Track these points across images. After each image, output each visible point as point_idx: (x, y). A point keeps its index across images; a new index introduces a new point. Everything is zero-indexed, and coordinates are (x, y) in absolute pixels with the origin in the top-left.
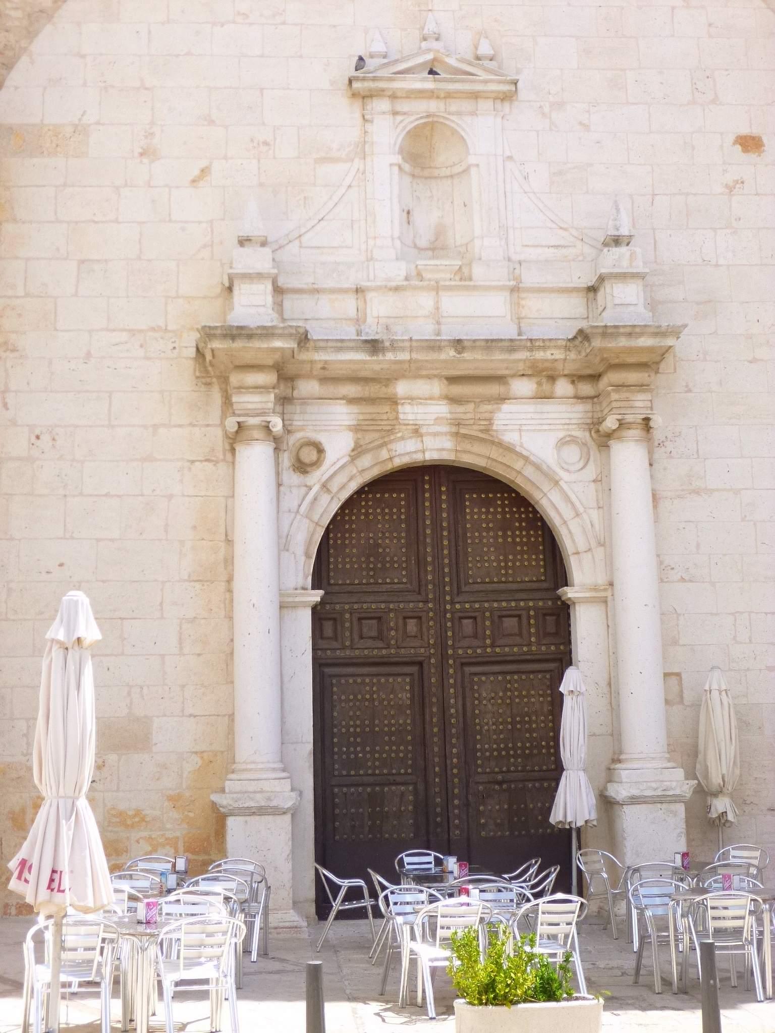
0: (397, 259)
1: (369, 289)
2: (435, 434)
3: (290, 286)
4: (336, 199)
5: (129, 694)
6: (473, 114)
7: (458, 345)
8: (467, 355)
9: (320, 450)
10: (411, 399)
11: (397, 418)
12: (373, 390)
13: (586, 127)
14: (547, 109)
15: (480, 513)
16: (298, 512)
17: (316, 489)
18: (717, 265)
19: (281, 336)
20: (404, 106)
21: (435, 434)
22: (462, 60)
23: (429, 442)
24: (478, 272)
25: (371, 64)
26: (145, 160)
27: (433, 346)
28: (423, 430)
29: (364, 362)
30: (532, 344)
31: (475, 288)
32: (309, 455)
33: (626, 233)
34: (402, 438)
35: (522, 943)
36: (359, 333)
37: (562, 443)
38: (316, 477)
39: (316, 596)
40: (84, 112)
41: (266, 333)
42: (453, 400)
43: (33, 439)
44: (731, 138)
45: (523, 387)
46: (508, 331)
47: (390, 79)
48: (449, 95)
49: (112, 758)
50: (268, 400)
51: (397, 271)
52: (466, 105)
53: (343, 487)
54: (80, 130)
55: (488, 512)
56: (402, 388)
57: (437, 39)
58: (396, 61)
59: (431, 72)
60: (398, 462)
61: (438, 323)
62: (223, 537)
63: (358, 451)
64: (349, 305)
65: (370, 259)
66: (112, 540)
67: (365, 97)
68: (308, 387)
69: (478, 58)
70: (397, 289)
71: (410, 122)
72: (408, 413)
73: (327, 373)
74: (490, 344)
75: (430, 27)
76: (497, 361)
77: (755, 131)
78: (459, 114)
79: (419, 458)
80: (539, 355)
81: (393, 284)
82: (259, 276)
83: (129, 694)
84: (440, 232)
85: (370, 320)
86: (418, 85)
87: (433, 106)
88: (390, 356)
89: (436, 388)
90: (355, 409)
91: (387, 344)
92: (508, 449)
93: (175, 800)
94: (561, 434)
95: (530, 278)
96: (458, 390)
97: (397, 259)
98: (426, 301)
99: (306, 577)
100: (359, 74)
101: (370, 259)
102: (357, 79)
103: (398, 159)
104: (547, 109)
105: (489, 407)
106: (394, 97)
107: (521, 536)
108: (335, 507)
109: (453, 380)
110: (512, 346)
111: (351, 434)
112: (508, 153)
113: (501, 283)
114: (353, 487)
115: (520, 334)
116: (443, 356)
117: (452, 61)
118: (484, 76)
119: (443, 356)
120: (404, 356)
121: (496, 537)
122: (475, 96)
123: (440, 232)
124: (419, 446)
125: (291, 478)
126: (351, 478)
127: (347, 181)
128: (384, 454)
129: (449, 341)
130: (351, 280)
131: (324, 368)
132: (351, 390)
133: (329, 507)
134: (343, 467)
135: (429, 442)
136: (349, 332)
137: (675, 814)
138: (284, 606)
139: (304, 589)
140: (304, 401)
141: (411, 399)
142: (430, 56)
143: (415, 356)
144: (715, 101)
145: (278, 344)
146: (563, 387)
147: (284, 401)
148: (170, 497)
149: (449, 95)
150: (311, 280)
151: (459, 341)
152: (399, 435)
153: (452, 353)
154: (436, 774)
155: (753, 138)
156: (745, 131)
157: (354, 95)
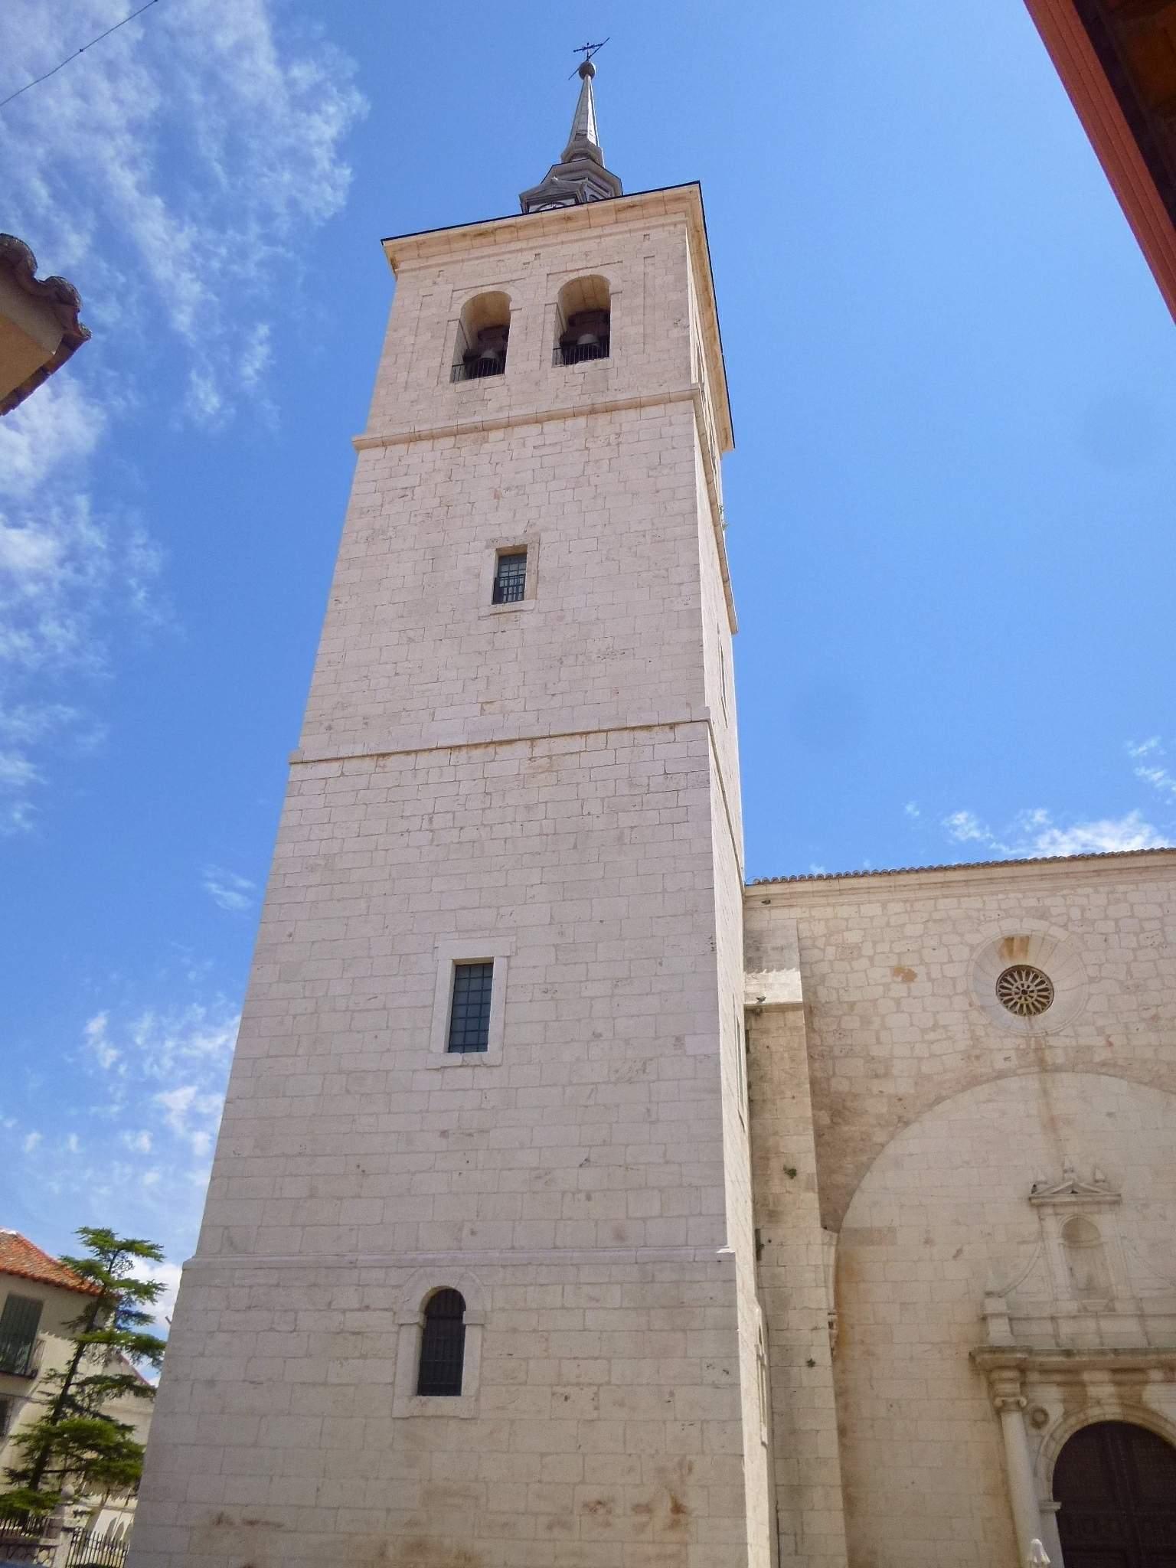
1: (1058, 1318)
2: (1110, 1404)
3: (1016, 1316)
6: (1099, 1212)
7: (1116, 1351)
8: (1122, 1358)
9: (1046, 1414)
10: (1093, 1383)
11: (1086, 1395)
13: (1164, 1218)
16: (1039, 1452)
17: (1047, 1439)
19: (1019, 1351)
20: (1060, 1210)
21: (1110, 1404)
22: (1088, 1184)
23: (1107, 1409)
24: (1118, 1306)
25: (1041, 1188)
26: (928, 1246)
27: (1102, 1353)
28: (1103, 1401)
29: (1062, 1362)
30: (1158, 1351)
31: (1119, 1316)
32: (1040, 1417)
34: (1091, 1407)
35: (1073, 933)
36: (1058, 1344)
38: (1046, 1431)
39: (1057, 1506)
40: (892, 1220)
41: (1013, 1349)
42: (1118, 1384)
46: (1141, 1343)
47: (1051, 1197)
48: (1083, 1204)
50: (1015, 1387)
51: (1072, 1307)
52: (1095, 1208)
53: (1062, 1437)
54: (892, 1230)
56: (1086, 1376)
57: (1072, 1171)
58: (1053, 1187)
59: (1073, 1192)
60: (1091, 1421)
61: (1101, 1337)
63: (1067, 1415)
64: (1049, 1327)
65: (1057, 1300)
67: (1040, 1206)
68: (1034, 1377)
69: (1097, 1181)
70: (1074, 1317)
71: (1066, 1219)
72: (1092, 1391)
74: (1134, 1351)
75: (1067, 1165)
76: (1139, 1361)
78: (1090, 1213)
79: (1102, 1418)
80: (1163, 1357)
82: (1000, 1315)
84: (1090, 1279)
86: (1068, 1199)
87: (1076, 1209)
88: (1077, 1358)
89: (1104, 1376)
90: (1061, 1389)
91: (1075, 1352)
92: (1154, 1413)
95: (1149, 1308)
96: (1119, 1377)
98: (1090, 1325)
99: (1049, 1493)
100: (1033, 1195)
101: (1057, 1300)
102: (1034, 1198)
103: (1061, 1241)
105: (1138, 1387)
106: (1054, 1205)
108: (1059, 1448)
109: (1115, 1371)
110: (1145, 1352)
111: (1061, 1405)
113: (1132, 1313)
114: (1067, 1436)
115: (1149, 1344)
116: (1108, 1358)
117: (1082, 1185)
118: (1103, 1193)
119: (1108, 1358)
120: (1085, 1358)
122: (1099, 1203)
123: (1090, 1279)
124: (1101, 1411)
125: (1033, 1431)
126: (1066, 1431)
127: (1036, 1254)
128: (1082, 1416)
129: (1111, 1349)
130: (1047, 1311)
131: (1040, 1365)
132: (1058, 1378)
133: (1056, 1449)
134: (1060, 1425)
135: (1107, 1409)
136: (1050, 1344)
138: (1042, 1512)
139: (1050, 1501)
140: (1033, 1384)
141: (1093, 1383)
142: (1071, 1183)
143: (1093, 1358)
145: (1019, 1355)
147: (1023, 1384)
149: (1083, 1204)
150: (1025, 1312)
151: (1116, 1350)
152: (1090, 1405)
153: (1113, 1356)
157: (1032, 1205)
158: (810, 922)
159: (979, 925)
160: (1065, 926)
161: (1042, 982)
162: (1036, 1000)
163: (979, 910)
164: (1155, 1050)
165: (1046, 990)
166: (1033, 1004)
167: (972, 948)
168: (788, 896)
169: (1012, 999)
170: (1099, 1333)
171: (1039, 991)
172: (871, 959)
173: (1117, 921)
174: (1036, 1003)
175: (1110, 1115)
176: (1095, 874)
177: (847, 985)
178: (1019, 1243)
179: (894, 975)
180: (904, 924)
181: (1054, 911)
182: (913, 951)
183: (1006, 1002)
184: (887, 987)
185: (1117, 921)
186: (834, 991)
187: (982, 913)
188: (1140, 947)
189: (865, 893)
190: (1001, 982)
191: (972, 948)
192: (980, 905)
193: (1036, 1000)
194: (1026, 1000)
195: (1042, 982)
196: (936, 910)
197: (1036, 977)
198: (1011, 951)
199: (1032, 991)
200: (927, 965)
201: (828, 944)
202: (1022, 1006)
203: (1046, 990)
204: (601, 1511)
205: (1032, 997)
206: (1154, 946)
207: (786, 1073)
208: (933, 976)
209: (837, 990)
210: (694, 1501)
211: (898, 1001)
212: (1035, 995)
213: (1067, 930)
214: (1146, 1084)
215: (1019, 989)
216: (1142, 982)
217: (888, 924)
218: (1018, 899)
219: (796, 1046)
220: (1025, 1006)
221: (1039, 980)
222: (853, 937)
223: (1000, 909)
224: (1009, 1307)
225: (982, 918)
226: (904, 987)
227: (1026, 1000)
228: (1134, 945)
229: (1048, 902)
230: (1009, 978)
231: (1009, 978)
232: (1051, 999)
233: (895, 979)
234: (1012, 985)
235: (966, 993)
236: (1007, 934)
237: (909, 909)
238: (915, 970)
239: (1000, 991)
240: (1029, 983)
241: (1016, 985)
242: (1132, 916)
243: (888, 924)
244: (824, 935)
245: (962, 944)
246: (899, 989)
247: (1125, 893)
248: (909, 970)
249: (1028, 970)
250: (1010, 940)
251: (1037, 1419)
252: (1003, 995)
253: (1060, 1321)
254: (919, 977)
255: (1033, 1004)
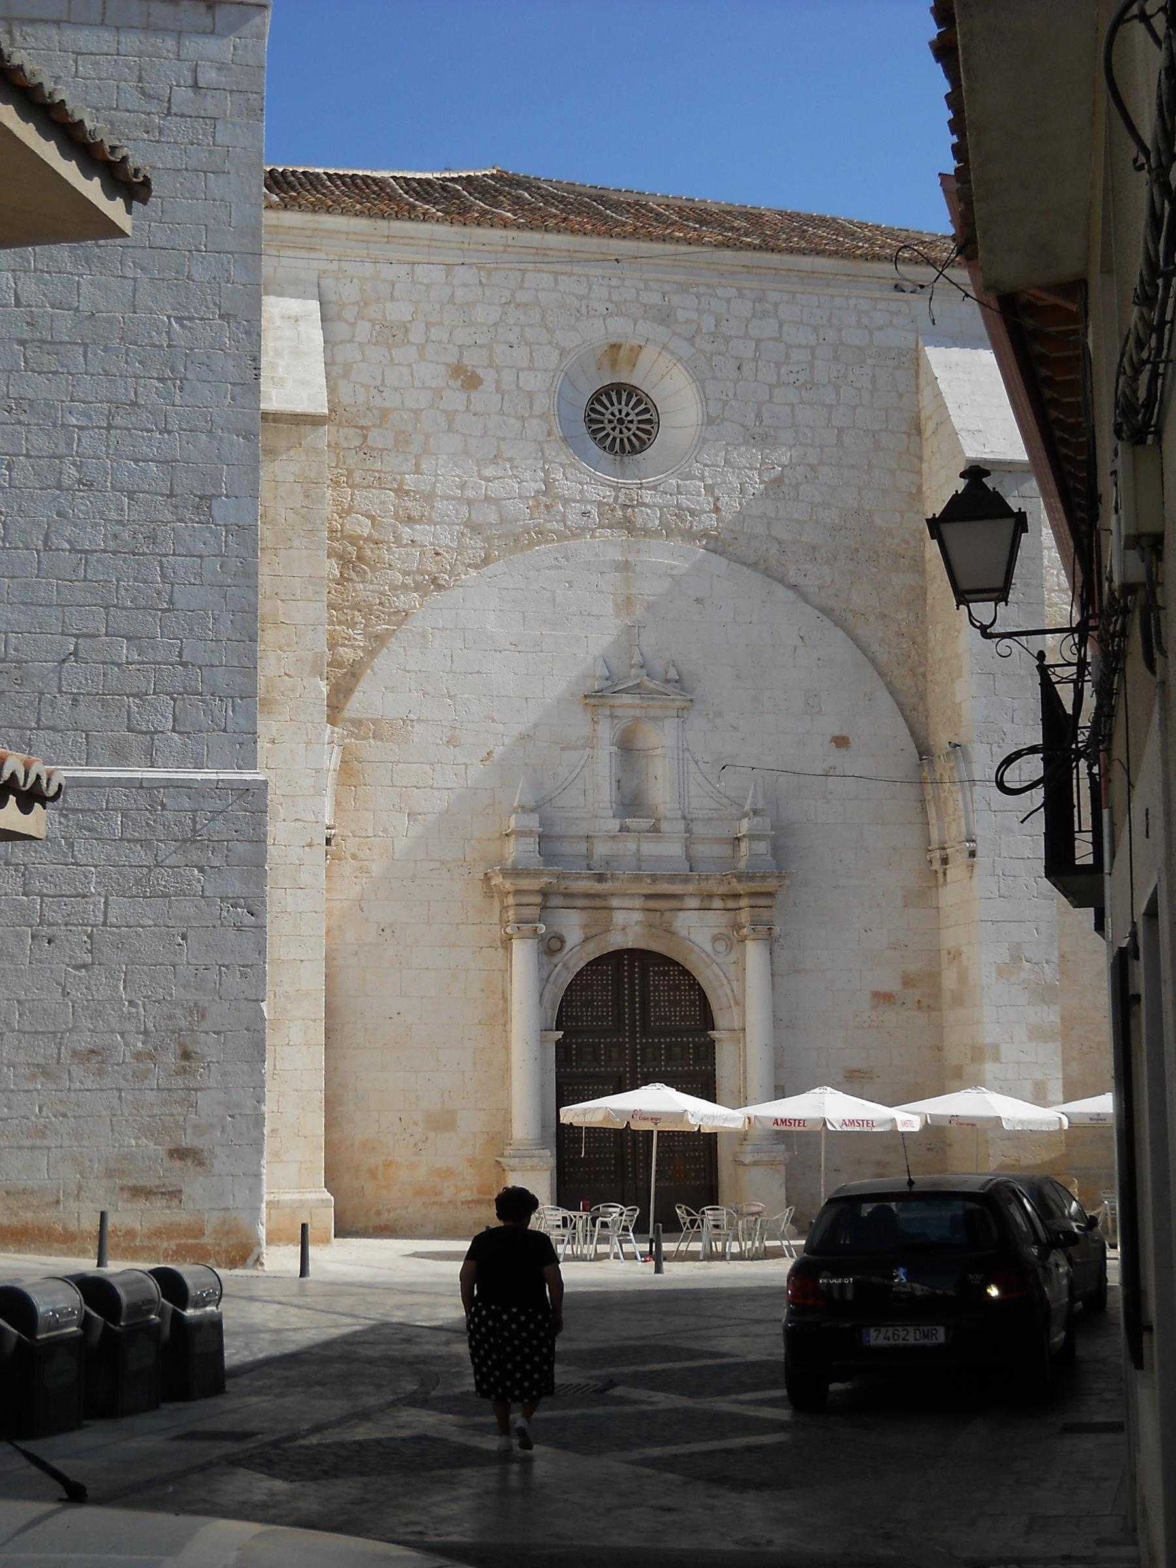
0: (614, 817)
4: (574, 775)
5: (442, 1096)
7: (654, 878)
12: (597, 903)
14: (711, 717)
15: (659, 980)
18: (816, 824)
32: (555, 944)
33: (761, 807)
37: (715, 939)
43: (380, 932)
44: (829, 738)
45: (693, 903)
49: (432, 1135)
55: (664, 980)
56: (615, 903)
62: (501, 996)
66: (431, 998)
73: (568, 891)
77: (844, 734)
81: (612, 834)
83: (442, 1096)
85: (595, 857)
88: (610, 884)
93: (472, 1162)
94: (716, 931)
97: (614, 817)
104: (711, 717)
107: (685, 996)
109: (648, 897)
112: (686, 746)
121: (669, 996)
125: (545, 959)
132: (581, 903)
137: (779, 1171)
144: (820, 712)
146: (717, 903)
147: (544, 907)
148: (468, 970)
154: (629, 1147)
155: (843, 738)
156: (837, 733)
158: (337, 279)
159: (578, 319)
160: (691, 340)
161: (646, 410)
162: (634, 434)
163: (581, 298)
164: (769, 524)
165: (649, 421)
166: (628, 439)
167: (563, 352)
168: (308, 233)
169: (603, 429)
170: (638, 856)
171: (639, 422)
172: (421, 348)
173: (758, 341)
174: (633, 438)
175: (698, 600)
176: (745, 270)
177: (383, 384)
178: (563, 749)
179: (451, 377)
180: (474, 303)
181: (681, 315)
182: (481, 346)
183: (595, 432)
184: (438, 393)
185: (758, 341)
186: (362, 390)
187: (584, 302)
188: (781, 384)
189: (424, 246)
190: (593, 404)
191: (563, 352)
192: (583, 290)
193: (634, 434)
194: (621, 432)
195: (646, 410)
196: (522, 288)
197: (639, 402)
198: (614, 363)
199: (631, 422)
200: (498, 370)
201: (359, 316)
202: (614, 439)
203: (649, 421)
204: (95, 1059)
205: (629, 430)
206: (796, 385)
207: (297, 513)
208: (505, 386)
209: (367, 387)
210: (208, 1046)
211: (451, 417)
212: (633, 427)
213: (693, 345)
214: (748, 565)
215: (615, 416)
216: (772, 433)
217: (452, 299)
218: (638, 290)
219: (313, 475)
220: (618, 440)
221: (642, 407)
222: (399, 312)
223: (612, 302)
224: (541, 824)
225: (584, 311)
226: (464, 397)
227: (621, 432)
228: (772, 380)
229: (676, 300)
230: (604, 399)
231: (604, 399)
232: (654, 435)
233: (451, 382)
234: (607, 409)
235: (542, 416)
236: (613, 340)
237: (484, 281)
238: (481, 372)
239: (589, 415)
240: (629, 409)
241: (611, 409)
242: (778, 339)
243: (452, 299)
244: (357, 303)
245: (550, 343)
246: (456, 399)
247: (776, 304)
248: (473, 373)
249: (632, 390)
250: (615, 347)
251: (551, 946)
252: (592, 421)
253: (595, 841)
254: (485, 383)
255: (628, 439)
